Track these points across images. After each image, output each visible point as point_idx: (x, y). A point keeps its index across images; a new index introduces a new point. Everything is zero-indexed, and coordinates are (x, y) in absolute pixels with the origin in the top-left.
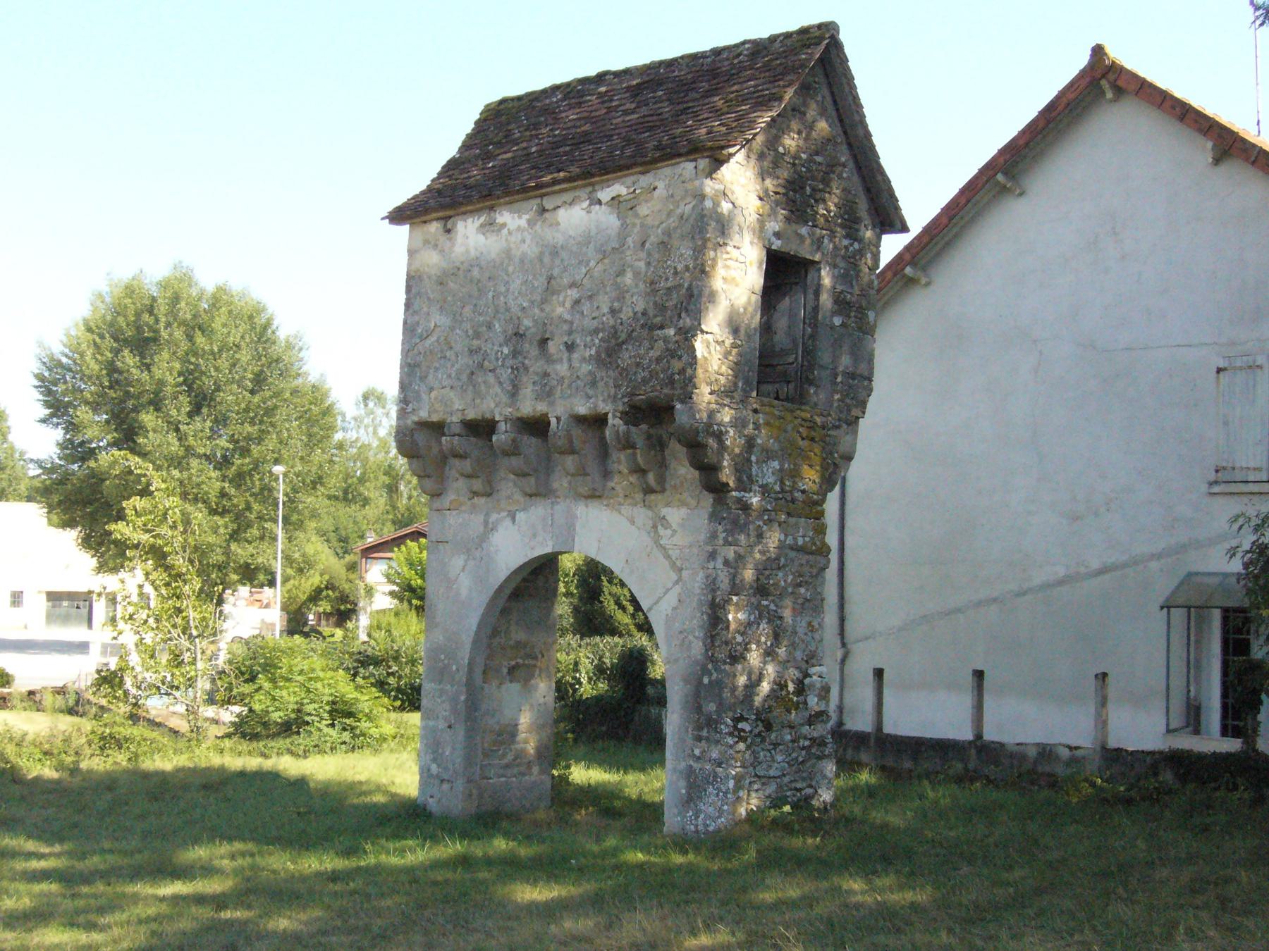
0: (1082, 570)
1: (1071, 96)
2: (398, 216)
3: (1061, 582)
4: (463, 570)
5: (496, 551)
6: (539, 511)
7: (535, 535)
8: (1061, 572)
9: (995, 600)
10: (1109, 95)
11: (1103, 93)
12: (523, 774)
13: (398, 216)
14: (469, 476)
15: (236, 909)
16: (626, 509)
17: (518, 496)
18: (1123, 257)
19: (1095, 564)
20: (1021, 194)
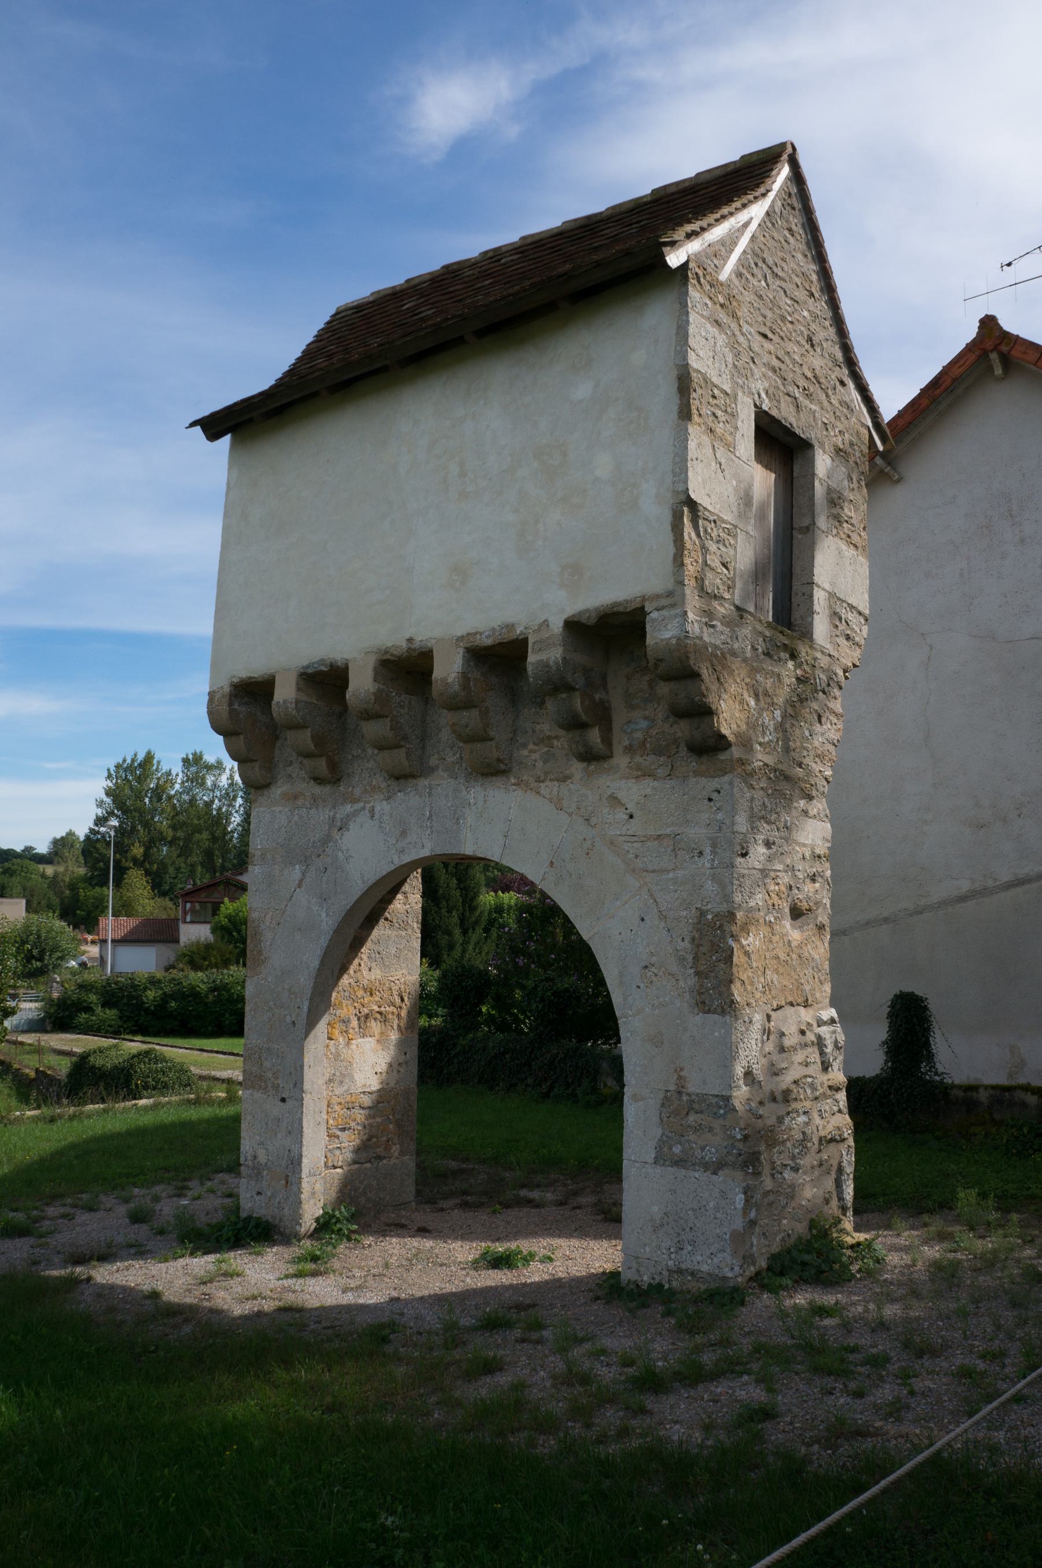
0: (990, 883)
1: (956, 372)
2: (213, 426)
3: (963, 899)
4: (300, 886)
5: (347, 859)
6: (409, 800)
7: (404, 833)
8: (965, 886)
9: (886, 920)
10: (998, 371)
11: (991, 369)
12: (380, 1158)
13: (213, 426)
14: (309, 755)
15: (59, 1102)
16: (549, 788)
17: (379, 780)
18: (1022, 541)
19: (1005, 877)
20: (898, 481)
